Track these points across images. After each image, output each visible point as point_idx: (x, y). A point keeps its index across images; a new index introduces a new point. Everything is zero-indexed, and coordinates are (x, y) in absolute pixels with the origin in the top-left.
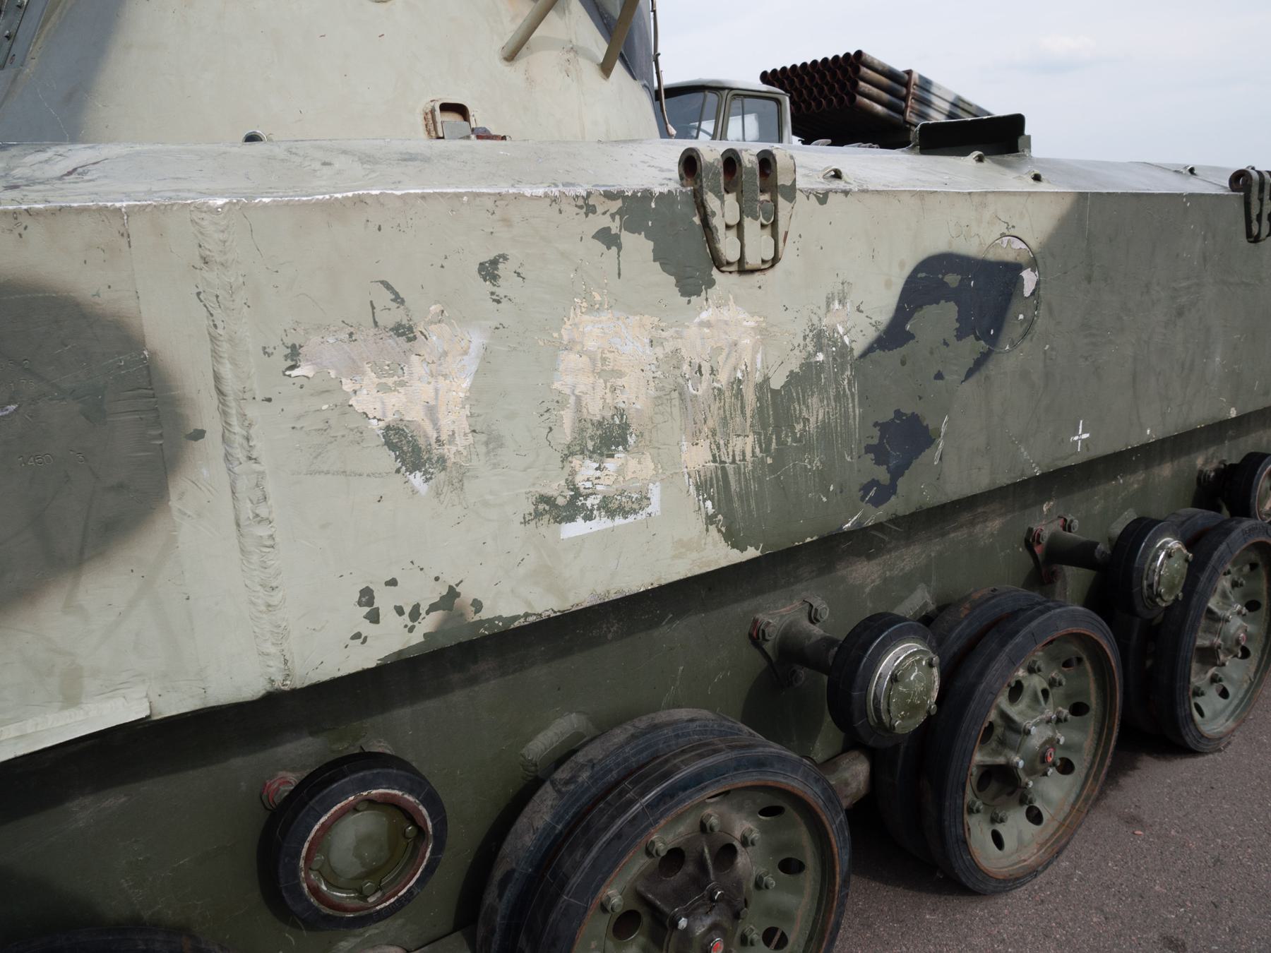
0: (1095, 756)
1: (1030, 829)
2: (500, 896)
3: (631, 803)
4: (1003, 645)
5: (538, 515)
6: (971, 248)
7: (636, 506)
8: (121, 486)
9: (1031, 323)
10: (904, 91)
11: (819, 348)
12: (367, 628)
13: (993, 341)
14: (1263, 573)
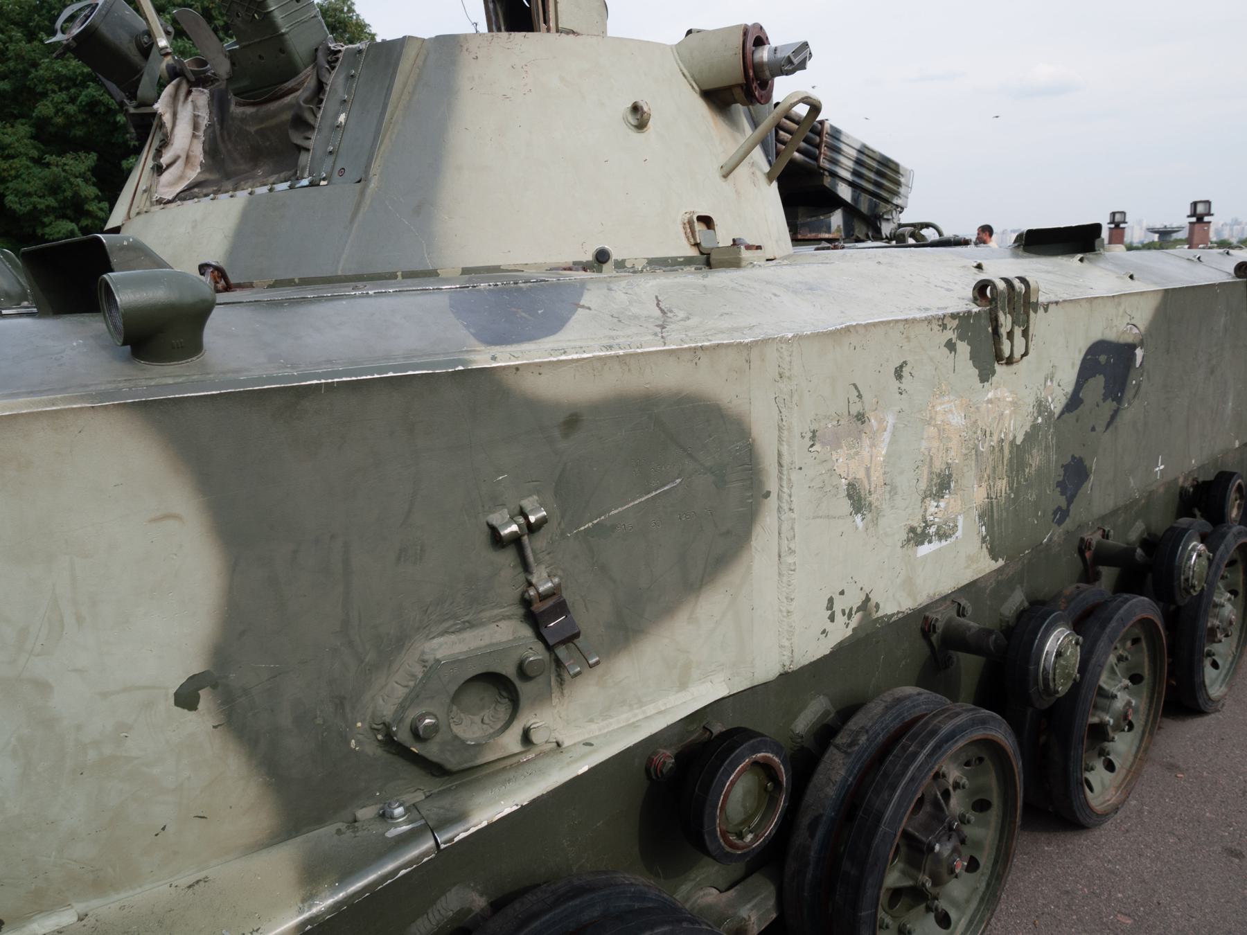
0: (1148, 715)
1: (1108, 775)
2: (812, 836)
3: (915, 755)
4: (1103, 627)
5: (909, 540)
6: (1111, 336)
7: (948, 532)
8: (728, 532)
9: (1139, 385)
10: (818, 139)
11: (1040, 414)
12: (829, 626)
13: (1119, 400)
14: (1240, 567)
